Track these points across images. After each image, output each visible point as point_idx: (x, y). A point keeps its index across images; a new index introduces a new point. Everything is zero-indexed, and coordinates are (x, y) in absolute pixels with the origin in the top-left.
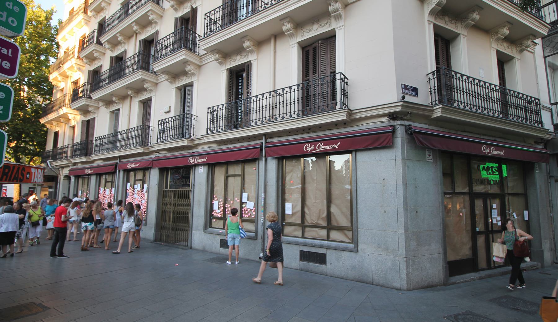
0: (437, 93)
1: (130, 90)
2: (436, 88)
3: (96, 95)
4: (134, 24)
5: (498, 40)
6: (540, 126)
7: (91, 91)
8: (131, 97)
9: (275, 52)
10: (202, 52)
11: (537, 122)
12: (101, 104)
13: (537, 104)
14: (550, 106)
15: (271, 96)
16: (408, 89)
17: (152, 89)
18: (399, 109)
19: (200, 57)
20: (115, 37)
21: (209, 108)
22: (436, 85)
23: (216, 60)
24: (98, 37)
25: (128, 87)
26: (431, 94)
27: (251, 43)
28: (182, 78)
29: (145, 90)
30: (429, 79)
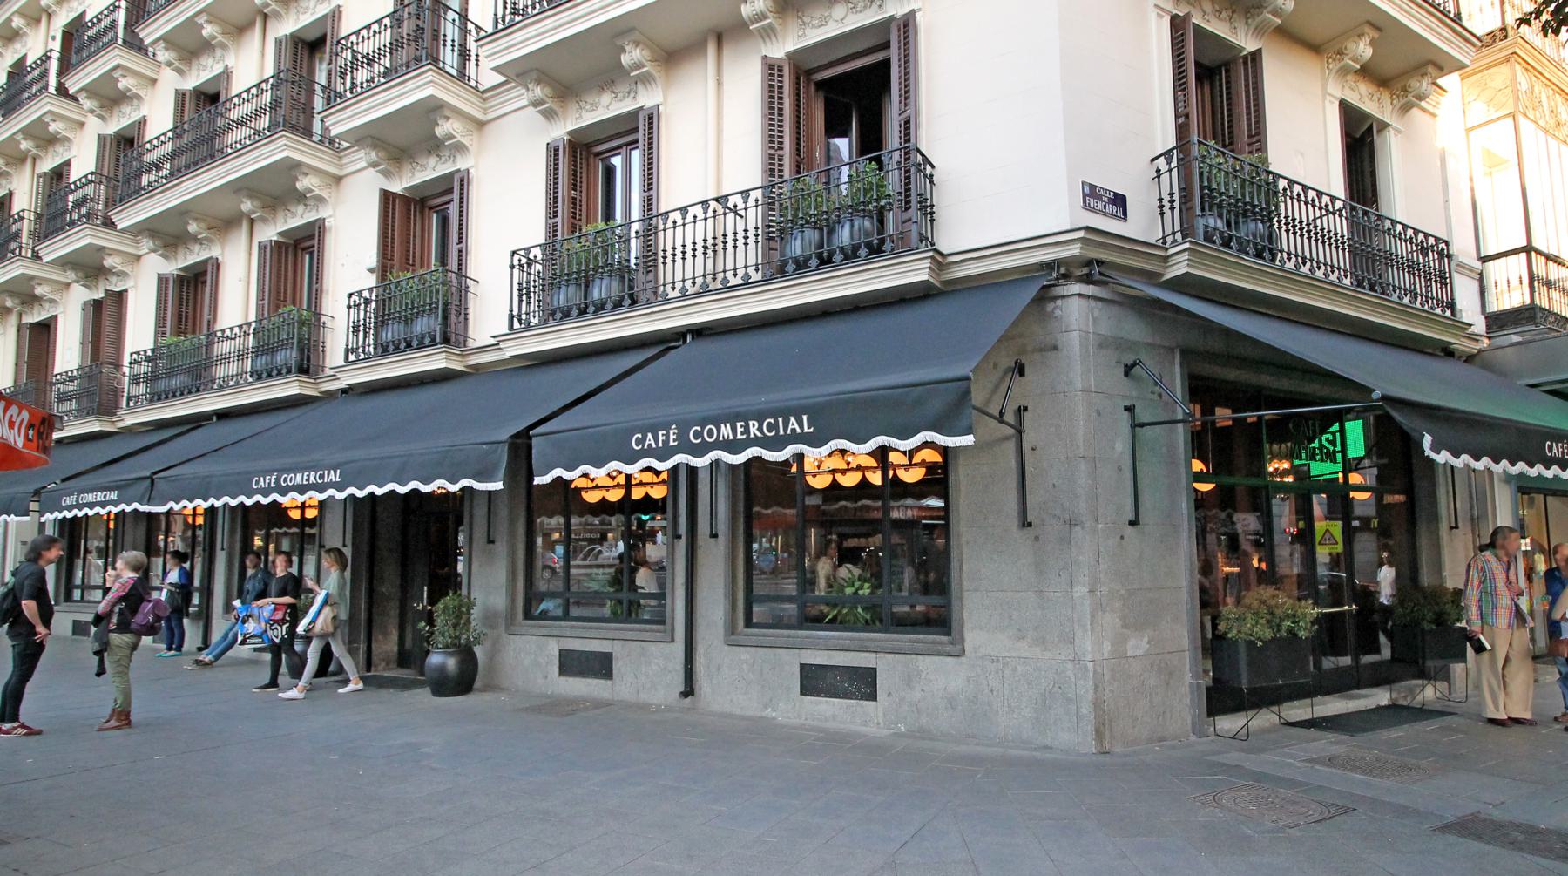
0: (1177, 211)
1: (250, 197)
2: (1176, 197)
3: (128, 217)
4: (19, 137)
5: (1344, 71)
6: (1448, 313)
7: (111, 203)
8: (252, 221)
9: (719, 83)
10: (489, 79)
11: (1440, 302)
12: (146, 245)
13: (1441, 253)
14: (1478, 265)
15: (710, 213)
16: (1099, 197)
17: (324, 194)
18: (1074, 251)
19: (483, 94)
20: (191, 24)
21: (514, 253)
22: (1176, 189)
23: (536, 104)
24: (128, 25)
25: (243, 187)
26: (1162, 214)
27: (646, 53)
28: (422, 161)
29: (302, 198)
30: (1158, 171)
